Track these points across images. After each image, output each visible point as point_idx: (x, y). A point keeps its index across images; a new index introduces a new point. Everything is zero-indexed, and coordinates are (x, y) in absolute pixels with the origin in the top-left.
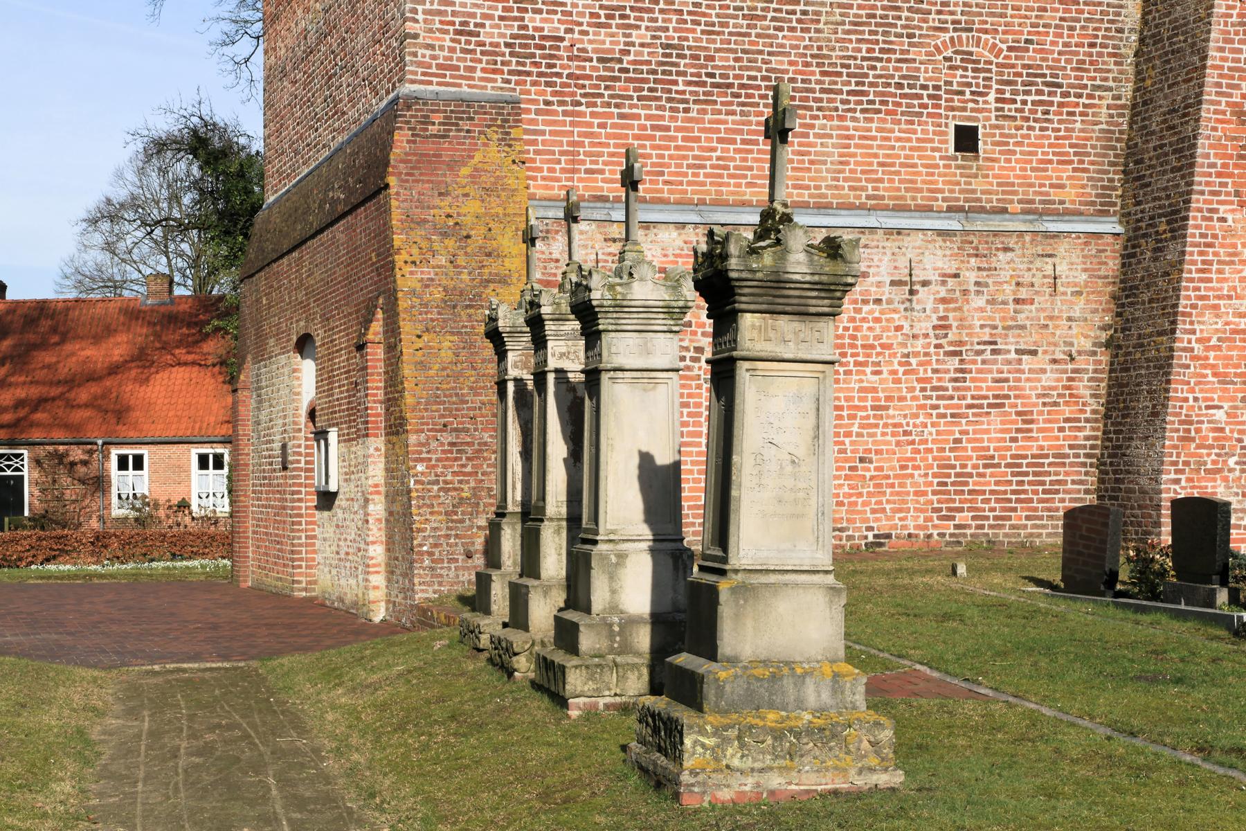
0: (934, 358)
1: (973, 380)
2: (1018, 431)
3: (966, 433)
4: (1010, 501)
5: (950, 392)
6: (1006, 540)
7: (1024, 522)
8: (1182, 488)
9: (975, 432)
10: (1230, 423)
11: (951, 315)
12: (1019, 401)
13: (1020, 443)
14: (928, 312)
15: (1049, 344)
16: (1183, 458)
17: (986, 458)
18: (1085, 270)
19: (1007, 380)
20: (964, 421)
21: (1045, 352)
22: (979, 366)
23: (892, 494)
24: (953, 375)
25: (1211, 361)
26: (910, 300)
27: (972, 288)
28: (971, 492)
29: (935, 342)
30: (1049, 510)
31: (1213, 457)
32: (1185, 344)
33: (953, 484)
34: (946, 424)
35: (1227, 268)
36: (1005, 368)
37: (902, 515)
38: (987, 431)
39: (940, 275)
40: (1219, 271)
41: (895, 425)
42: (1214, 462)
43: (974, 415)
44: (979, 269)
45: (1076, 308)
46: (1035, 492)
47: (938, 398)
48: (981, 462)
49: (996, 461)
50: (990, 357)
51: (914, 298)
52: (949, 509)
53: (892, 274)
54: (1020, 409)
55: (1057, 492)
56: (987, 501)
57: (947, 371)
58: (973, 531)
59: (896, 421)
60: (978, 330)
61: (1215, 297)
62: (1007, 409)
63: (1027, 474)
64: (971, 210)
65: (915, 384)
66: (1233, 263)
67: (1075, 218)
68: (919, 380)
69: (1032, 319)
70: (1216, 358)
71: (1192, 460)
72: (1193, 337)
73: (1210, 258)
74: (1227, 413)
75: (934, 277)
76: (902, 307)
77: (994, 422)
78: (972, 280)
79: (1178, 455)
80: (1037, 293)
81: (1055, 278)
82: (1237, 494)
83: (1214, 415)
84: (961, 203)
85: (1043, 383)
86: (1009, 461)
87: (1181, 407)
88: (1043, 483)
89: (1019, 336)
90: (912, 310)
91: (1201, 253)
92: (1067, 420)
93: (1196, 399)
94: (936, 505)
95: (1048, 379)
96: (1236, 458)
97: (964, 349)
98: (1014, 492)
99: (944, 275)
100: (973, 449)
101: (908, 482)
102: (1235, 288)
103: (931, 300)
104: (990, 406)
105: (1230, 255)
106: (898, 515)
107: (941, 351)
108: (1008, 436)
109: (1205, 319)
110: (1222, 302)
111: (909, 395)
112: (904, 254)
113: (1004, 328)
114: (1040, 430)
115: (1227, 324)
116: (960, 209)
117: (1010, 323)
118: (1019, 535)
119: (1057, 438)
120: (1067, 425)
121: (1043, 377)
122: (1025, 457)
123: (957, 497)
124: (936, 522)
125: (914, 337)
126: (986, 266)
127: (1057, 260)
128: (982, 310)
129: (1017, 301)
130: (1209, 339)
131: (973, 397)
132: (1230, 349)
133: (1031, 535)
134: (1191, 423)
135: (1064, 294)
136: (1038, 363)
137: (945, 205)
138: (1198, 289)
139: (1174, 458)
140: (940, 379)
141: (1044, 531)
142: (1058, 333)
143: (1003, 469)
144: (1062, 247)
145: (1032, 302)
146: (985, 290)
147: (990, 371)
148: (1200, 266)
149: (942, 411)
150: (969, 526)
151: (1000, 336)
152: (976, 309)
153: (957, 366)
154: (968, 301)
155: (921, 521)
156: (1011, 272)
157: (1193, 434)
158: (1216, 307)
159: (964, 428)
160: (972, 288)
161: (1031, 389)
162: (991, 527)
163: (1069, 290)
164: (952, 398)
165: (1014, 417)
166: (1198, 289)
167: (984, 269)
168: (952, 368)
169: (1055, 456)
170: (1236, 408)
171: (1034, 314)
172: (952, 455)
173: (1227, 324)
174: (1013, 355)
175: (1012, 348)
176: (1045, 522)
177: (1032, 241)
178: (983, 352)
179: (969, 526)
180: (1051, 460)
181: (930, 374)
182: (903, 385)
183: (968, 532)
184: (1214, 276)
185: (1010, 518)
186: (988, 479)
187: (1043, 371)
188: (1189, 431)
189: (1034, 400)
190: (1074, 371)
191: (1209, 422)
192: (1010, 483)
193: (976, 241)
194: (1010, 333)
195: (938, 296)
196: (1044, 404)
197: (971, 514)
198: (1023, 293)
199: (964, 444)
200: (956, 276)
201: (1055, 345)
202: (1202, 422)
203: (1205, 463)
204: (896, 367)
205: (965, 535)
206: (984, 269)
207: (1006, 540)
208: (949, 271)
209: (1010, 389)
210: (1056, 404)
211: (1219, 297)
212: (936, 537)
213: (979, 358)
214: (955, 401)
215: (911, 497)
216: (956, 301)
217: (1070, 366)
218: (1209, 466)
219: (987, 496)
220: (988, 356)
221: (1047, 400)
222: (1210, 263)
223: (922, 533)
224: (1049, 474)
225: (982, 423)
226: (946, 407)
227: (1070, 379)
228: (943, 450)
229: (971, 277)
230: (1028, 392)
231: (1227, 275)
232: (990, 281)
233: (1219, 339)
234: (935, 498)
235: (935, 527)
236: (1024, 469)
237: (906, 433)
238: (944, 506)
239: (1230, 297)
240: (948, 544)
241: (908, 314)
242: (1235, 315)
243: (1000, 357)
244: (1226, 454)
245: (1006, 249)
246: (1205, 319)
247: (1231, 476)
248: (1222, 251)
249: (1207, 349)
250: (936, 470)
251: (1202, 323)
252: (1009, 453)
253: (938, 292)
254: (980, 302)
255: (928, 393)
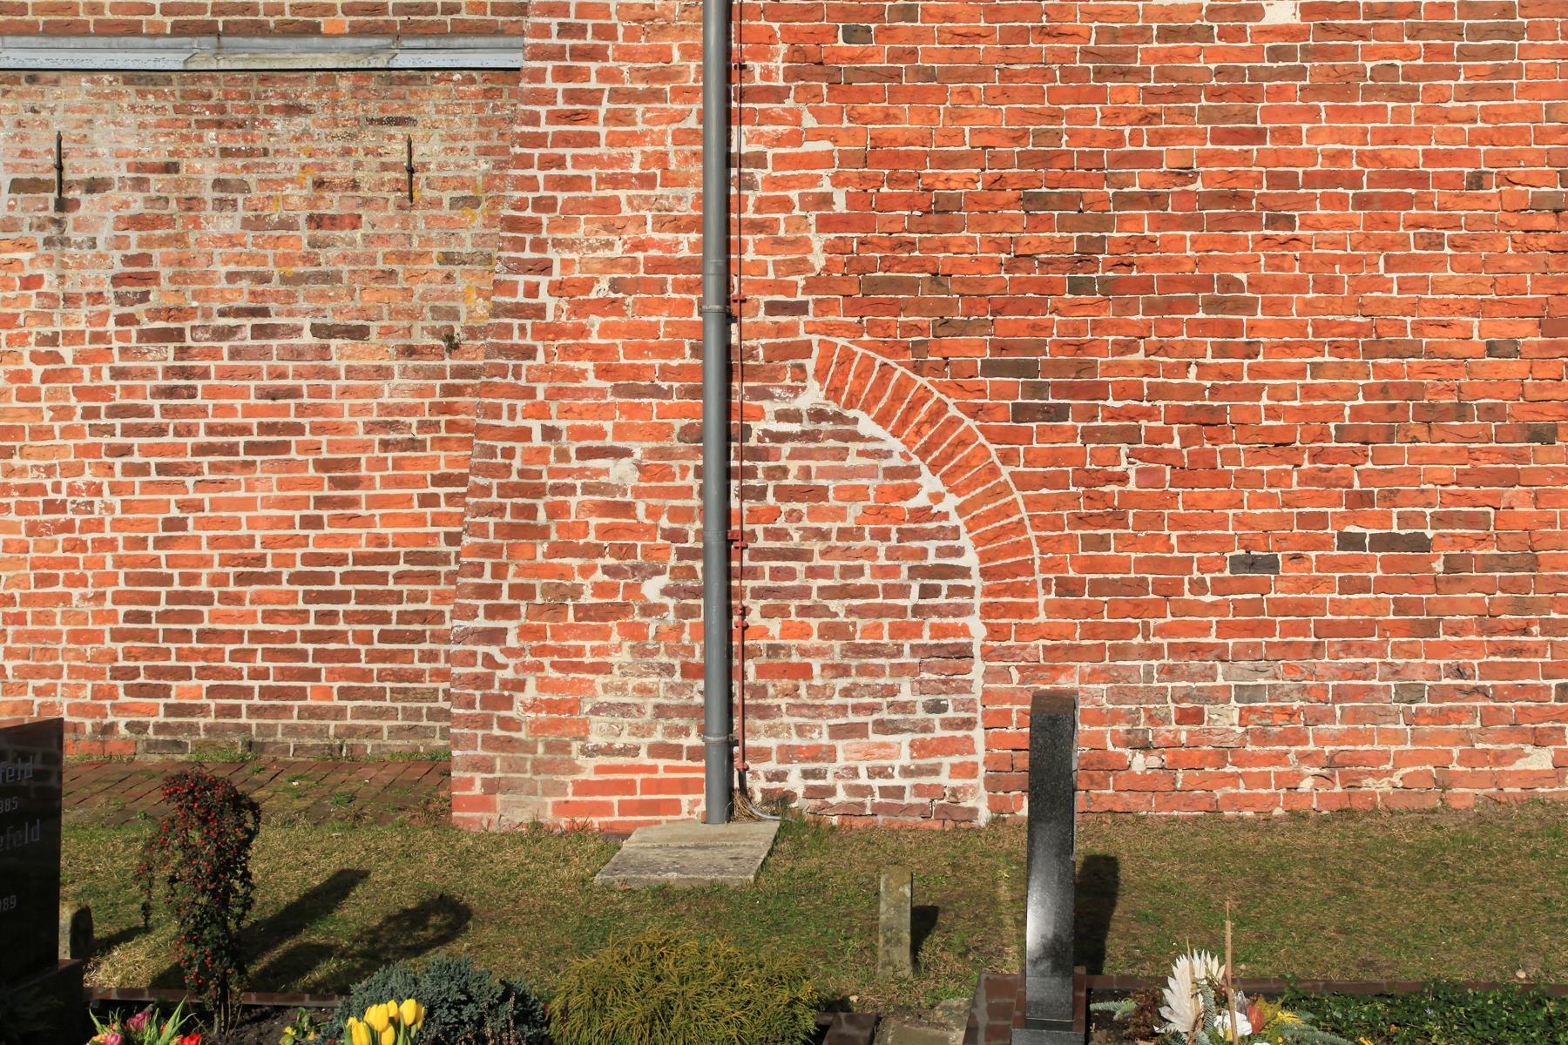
0: (116, 345)
1: (211, 392)
2: (321, 502)
3: (198, 506)
4: (302, 655)
5: (157, 419)
6: (292, 742)
7: (336, 702)
8: (510, 653)
9: (215, 505)
10: (649, 493)
11: (156, 253)
12: (324, 439)
13: (327, 530)
14: (101, 246)
15: (395, 313)
16: (511, 578)
17: (246, 561)
18: (485, 152)
19: (294, 393)
20: (190, 481)
21: (387, 332)
22: (226, 362)
23: (18, 637)
24: (161, 382)
25: (594, 339)
26: (59, 223)
27: (209, 194)
28: (204, 636)
29: (117, 310)
30: (398, 676)
31: (599, 576)
32: (521, 298)
33: (163, 617)
34: (146, 487)
35: (640, 108)
36: (290, 366)
37: (42, 683)
38: (248, 504)
39: (129, 167)
40: (614, 118)
41: (25, 490)
42: (599, 589)
43: (214, 467)
44: (226, 153)
45: (465, 234)
46: (365, 638)
47: (128, 431)
48: (231, 570)
49: (269, 568)
50: (249, 342)
51: (70, 217)
52: (154, 672)
53: (15, 168)
54: (325, 455)
55: (418, 637)
56: (247, 655)
57: (149, 373)
58: (211, 720)
59: (28, 480)
60: (223, 284)
61: (602, 181)
62: (293, 455)
63: (343, 597)
64: (232, 30)
65: (73, 401)
66: (657, 96)
67: (481, 41)
68: (81, 393)
69: (356, 260)
70: (605, 331)
71: (539, 583)
72: (544, 281)
73: (593, 84)
74: (640, 468)
75: (117, 172)
76: (39, 237)
77: (265, 482)
78: (210, 176)
79: (499, 571)
80: (367, 202)
81: (411, 171)
82: (668, 670)
83: (606, 472)
84: (208, 17)
85: (385, 400)
86: (300, 567)
87: (509, 453)
88: (384, 618)
89: (322, 296)
90: (65, 242)
91: (563, 74)
92: (440, 480)
93: (550, 433)
94: (121, 663)
95: (396, 390)
96: (664, 580)
97: (187, 325)
98: (309, 637)
99: (141, 167)
100: (214, 542)
101: (58, 611)
102: (662, 159)
103: (110, 223)
104: (251, 448)
105: (649, 76)
106: (32, 683)
107: (134, 330)
108: (297, 514)
109: (579, 234)
110: (622, 194)
111: (57, 426)
112: (45, 125)
113: (285, 280)
114: (374, 502)
115: (639, 246)
116: (208, 29)
117: (301, 269)
118: (323, 732)
119: (419, 520)
120: (442, 491)
121: (386, 386)
122: (340, 560)
123: (173, 646)
124: (123, 698)
125: (70, 300)
126: (242, 145)
127: (417, 132)
128: (231, 240)
129: (316, 221)
130: (587, 285)
131: (211, 430)
132: (645, 307)
133: (352, 731)
134: (538, 491)
135: (437, 203)
136: (372, 355)
137: (169, 20)
138: (559, 162)
139: (487, 578)
140: (129, 392)
141: (385, 724)
142: (419, 289)
143: (285, 586)
144: (430, 103)
145: (355, 222)
146: (240, 198)
147: (254, 374)
148: (561, 105)
149: (137, 458)
150: (203, 710)
151: (276, 296)
152: (218, 241)
153: (171, 362)
154: (198, 226)
155: (86, 696)
156: (304, 159)
157: (542, 517)
158: (610, 205)
159: (192, 495)
160: (209, 194)
161: (354, 411)
162: (254, 711)
163: (446, 197)
164: (160, 431)
165: (311, 472)
166: (559, 162)
167: (238, 153)
168: (159, 366)
169: (412, 558)
170: (667, 454)
171: (360, 248)
172: (162, 553)
173: (639, 246)
174: (307, 338)
175: (306, 323)
176: (387, 703)
177: (355, 92)
178: (230, 332)
179: (203, 710)
180: (403, 566)
181: (106, 380)
182: (43, 404)
183: (202, 721)
184: (602, 130)
185: (301, 694)
186: (248, 607)
187: (384, 373)
188: (531, 511)
189: (361, 435)
190: (459, 372)
191: (587, 489)
192: (302, 616)
193: (217, 94)
194: (301, 290)
195: (125, 213)
196: (385, 445)
197: (206, 683)
198: (333, 204)
199: (191, 531)
200: (170, 168)
201: (412, 315)
202: (571, 490)
203: (576, 591)
204: (27, 364)
205: (193, 729)
206: (238, 153)
207: (292, 742)
208: (154, 159)
209: (301, 410)
210: (414, 444)
211: (614, 182)
212: (123, 731)
213: (225, 346)
214: (170, 438)
215: (64, 644)
216: (170, 222)
217: (448, 362)
218: (588, 598)
219: (246, 645)
220: (246, 340)
221: (393, 436)
222: (594, 97)
223: (88, 723)
224: (397, 597)
225: (236, 486)
226: (147, 451)
227: (449, 390)
228: (142, 543)
229: (208, 169)
230: (347, 418)
231: (640, 127)
232: (251, 178)
233: (615, 285)
234: (119, 647)
235: (120, 709)
236: (338, 586)
237: (50, 506)
238: (141, 664)
239: (647, 181)
240: (152, 746)
241: (54, 251)
242: (660, 224)
243: (274, 343)
244: (634, 568)
245: (292, 110)
246: (579, 234)
247: (652, 625)
248: (625, 67)
249: (579, 309)
250: (122, 586)
251: (571, 245)
252: (299, 552)
253: (126, 204)
254: (228, 224)
255: (104, 421)
